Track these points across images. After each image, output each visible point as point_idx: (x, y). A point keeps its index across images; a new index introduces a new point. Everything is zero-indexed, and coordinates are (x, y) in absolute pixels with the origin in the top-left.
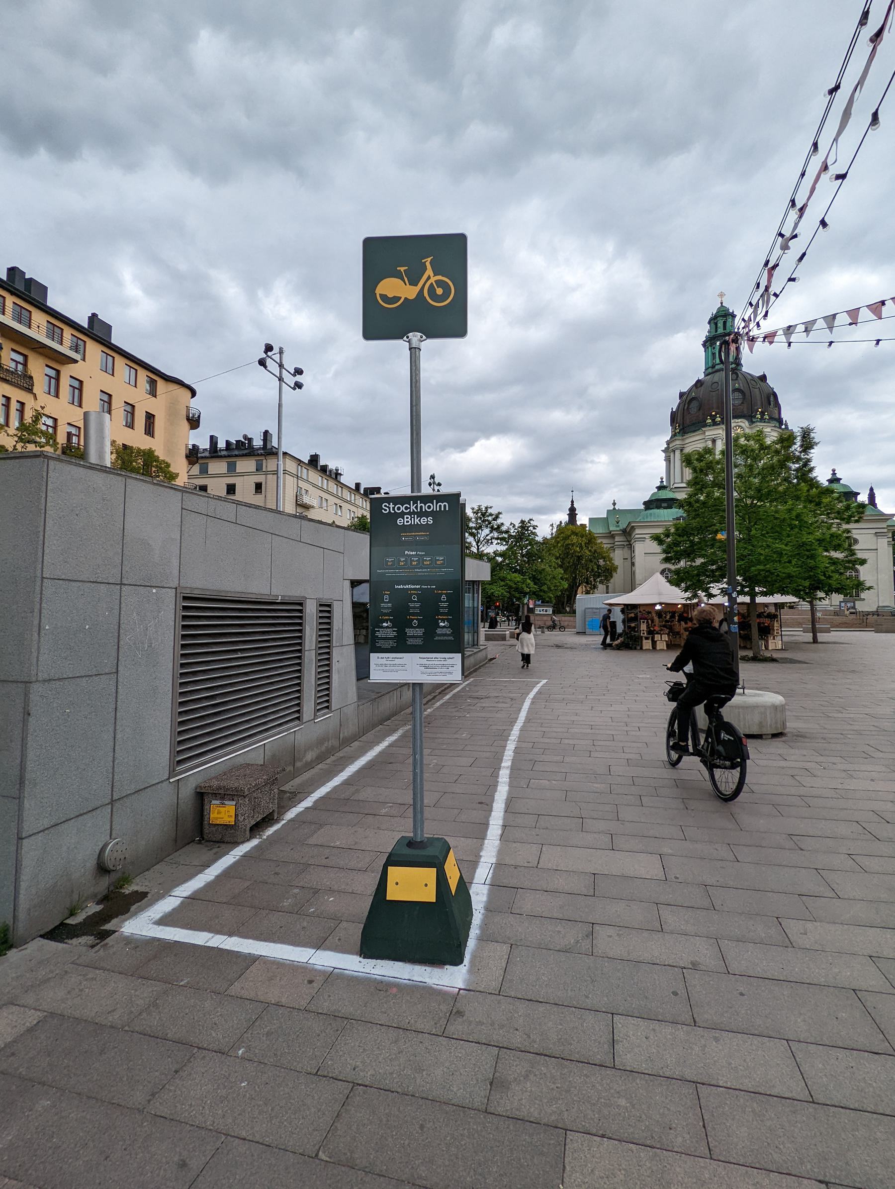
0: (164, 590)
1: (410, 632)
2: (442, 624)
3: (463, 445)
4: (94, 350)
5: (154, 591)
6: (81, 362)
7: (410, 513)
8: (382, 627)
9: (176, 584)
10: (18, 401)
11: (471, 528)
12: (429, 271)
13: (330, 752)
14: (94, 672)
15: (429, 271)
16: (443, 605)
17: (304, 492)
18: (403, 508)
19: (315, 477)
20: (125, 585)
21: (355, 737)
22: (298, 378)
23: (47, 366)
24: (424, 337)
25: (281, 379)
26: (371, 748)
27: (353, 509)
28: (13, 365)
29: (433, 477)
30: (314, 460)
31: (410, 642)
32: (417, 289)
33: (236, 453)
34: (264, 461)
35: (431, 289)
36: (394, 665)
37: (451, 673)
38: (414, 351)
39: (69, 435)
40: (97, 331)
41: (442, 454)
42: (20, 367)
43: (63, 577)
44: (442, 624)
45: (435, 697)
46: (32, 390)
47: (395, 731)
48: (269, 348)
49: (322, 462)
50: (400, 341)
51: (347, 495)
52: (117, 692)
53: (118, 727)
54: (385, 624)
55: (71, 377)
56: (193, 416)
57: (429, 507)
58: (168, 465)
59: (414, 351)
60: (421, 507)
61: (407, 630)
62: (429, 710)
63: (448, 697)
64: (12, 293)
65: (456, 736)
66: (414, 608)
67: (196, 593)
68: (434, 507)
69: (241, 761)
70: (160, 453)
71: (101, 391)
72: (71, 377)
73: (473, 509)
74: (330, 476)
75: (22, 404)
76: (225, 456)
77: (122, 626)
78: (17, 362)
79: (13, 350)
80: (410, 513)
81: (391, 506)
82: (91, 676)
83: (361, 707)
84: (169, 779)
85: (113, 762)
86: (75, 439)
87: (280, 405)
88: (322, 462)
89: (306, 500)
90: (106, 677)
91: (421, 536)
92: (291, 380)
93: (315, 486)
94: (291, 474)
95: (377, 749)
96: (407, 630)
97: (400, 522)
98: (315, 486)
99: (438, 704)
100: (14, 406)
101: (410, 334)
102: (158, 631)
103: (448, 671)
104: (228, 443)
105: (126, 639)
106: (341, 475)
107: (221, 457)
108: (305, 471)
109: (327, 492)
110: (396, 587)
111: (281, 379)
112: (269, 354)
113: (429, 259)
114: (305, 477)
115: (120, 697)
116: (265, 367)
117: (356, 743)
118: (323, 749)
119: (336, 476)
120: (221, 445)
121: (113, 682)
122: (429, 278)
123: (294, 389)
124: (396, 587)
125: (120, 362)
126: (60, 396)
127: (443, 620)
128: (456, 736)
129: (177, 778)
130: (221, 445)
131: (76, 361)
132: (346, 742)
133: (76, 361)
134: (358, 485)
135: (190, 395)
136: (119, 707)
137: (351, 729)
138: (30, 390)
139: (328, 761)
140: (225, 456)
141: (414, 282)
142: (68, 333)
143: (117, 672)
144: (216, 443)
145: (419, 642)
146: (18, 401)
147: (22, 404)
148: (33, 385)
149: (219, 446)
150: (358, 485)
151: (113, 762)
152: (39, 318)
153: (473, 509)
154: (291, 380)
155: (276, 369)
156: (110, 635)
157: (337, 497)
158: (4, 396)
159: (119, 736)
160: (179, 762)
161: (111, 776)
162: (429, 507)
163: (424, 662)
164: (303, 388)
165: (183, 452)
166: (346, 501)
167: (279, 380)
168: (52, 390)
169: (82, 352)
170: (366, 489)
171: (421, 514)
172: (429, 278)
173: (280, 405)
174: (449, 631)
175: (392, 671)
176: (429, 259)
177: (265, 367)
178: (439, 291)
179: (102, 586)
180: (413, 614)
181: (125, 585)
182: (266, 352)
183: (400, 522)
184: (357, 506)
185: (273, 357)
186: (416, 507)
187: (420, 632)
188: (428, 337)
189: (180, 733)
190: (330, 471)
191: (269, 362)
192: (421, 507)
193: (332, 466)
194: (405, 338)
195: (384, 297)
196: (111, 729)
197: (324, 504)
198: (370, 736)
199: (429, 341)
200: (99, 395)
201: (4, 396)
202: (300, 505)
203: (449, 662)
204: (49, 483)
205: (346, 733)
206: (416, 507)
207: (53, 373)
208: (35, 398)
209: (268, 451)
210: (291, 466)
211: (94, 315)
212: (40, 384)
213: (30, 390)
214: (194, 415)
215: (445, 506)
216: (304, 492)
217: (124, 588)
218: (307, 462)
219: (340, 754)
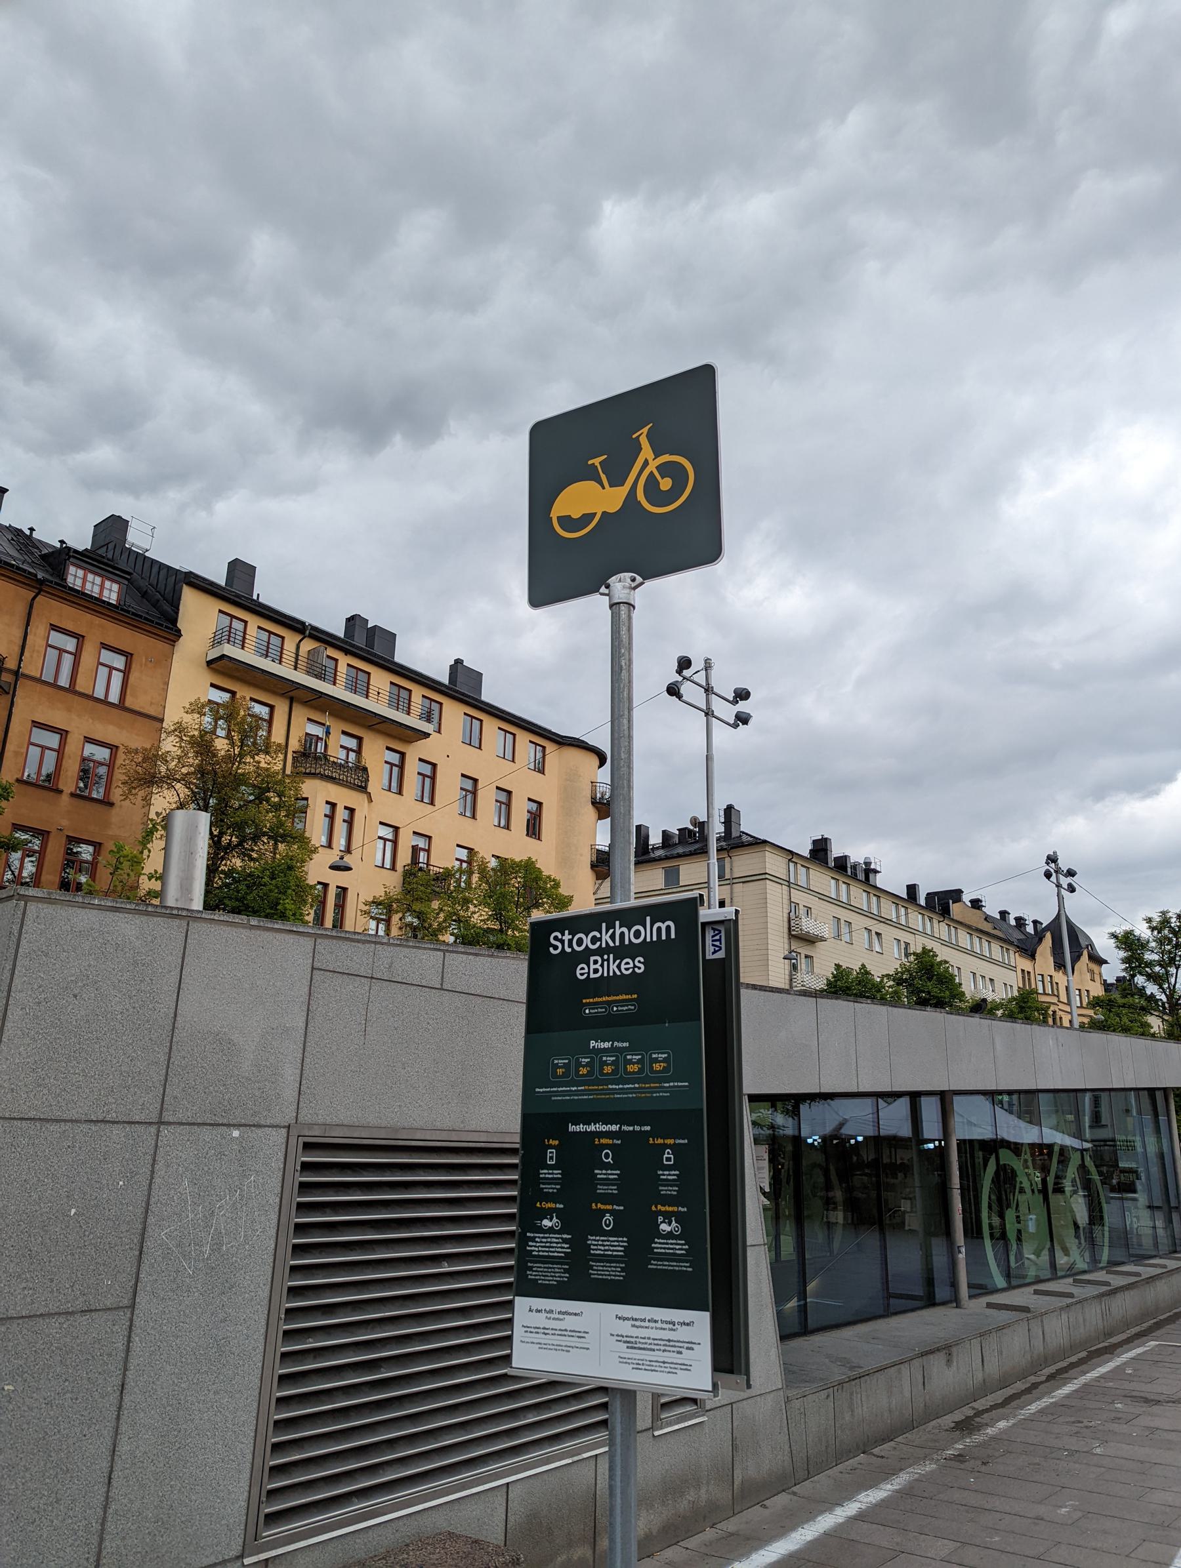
0: (259, 1131)
1: (598, 1245)
2: (664, 1227)
3: (1145, 785)
4: (454, 714)
5: (236, 1133)
6: (434, 735)
7: (600, 952)
8: (541, 1230)
9: (289, 1117)
10: (346, 808)
11: (1150, 964)
12: (647, 452)
13: (707, 1515)
14: (79, 1304)
15: (647, 452)
16: (665, 1175)
17: (802, 911)
18: (587, 941)
19: (822, 880)
20: (169, 1123)
21: (782, 1482)
22: (742, 706)
23: (388, 748)
24: (639, 579)
25: (709, 713)
26: (811, 1516)
27: (905, 937)
28: (342, 754)
29: (1052, 859)
30: (820, 849)
31: (600, 1271)
32: (622, 492)
33: (680, 850)
34: (727, 860)
35: (652, 482)
36: (563, 1332)
37: (686, 1367)
38: (620, 611)
39: (415, 850)
40: (462, 686)
41: (1098, 806)
42: (352, 756)
43: (32, 1114)
44: (664, 1227)
45: (1035, 1386)
46: (366, 788)
47: (888, 1474)
48: (684, 664)
49: (836, 851)
50: (596, 597)
51: (889, 910)
52: (128, 1350)
53: (124, 1428)
54: (546, 1223)
55: (420, 760)
56: (602, 798)
57: (637, 934)
58: (557, 885)
59: (620, 611)
60: (622, 934)
61: (592, 1240)
62: (1002, 1424)
63: (1067, 1389)
64: (347, 652)
65: (1042, 1510)
66: (607, 1182)
67: (337, 1136)
68: (648, 932)
69: (441, 1523)
70: (548, 866)
71: (463, 775)
72: (420, 760)
73: (1149, 920)
74: (854, 877)
75: (352, 811)
76: (660, 859)
77: (153, 1207)
78: (348, 750)
79: (344, 733)
80: (600, 952)
81: (567, 937)
82: (72, 1313)
83: (797, 1404)
84: (241, 1556)
85: (105, 1508)
86: (422, 857)
87: (709, 758)
88: (836, 851)
89: (808, 925)
90: (105, 1315)
91: (623, 1003)
92: (726, 711)
93: (823, 897)
94: (777, 880)
95: (826, 1522)
96: (592, 1240)
97: (581, 972)
98: (823, 897)
99: (1034, 1408)
100: (341, 814)
101: (612, 580)
102: (241, 1218)
103: (678, 1359)
104: (666, 835)
105: (159, 1235)
106: (876, 872)
107: (655, 860)
108: (802, 871)
109: (849, 907)
110: (572, 1128)
111: (709, 713)
112: (686, 673)
113: (645, 430)
114: (802, 881)
115: (133, 1362)
116: (679, 697)
117: (782, 1500)
118: (683, 1505)
119: (865, 875)
120: (655, 839)
121: (121, 1330)
122: (646, 463)
123: (735, 726)
124: (572, 1128)
125: (491, 726)
126: (404, 793)
127: (668, 1217)
128: (1042, 1510)
129: (263, 1556)
130: (655, 839)
131: (427, 735)
132: (753, 1493)
133: (427, 735)
134: (912, 890)
135: (597, 763)
136: (130, 1383)
137: (765, 1459)
138: (363, 788)
139: (693, 1542)
140: (660, 859)
141: (617, 480)
142: (418, 692)
143: (133, 1306)
144: (647, 837)
145: (614, 1272)
146: (346, 808)
147: (352, 811)
148: (367, 780)
149: (651, 842)
150: (912, 890)
151: (105, 1508)
152: (380, 680)
153: (1149, 920)
154: (726, 711)
155: (698, 697)
156: (124, 1228)
157: (868, 914)
158: (327, 802)
159: (124, 1447)
160: (273, 1518)
161: (95, 1540)
162: (637, 934)
163: (626, 1328)
164: (751, 722)
165: (587, 858)
166: (886, 921)
167: (707, 714)
168: (394, 784)
169: (436, 720)
170: (930, 896)
171: (622, 951)
172: (646, 463)
173: (709, 758)
174: (680, 1247)
175: (558, 1348)
176: (645, 430)
177: (679, 697)
178: (666, 484)
179: (116, 1130)
180: (606, 1198)
181: (169, 1123)
182: (679, 672)
183: (581, 972)
184: (913, 932)
185: (696, 678)
186: (613, 937)
187: (616, 1246)
188: (646, 577)
189: (277, 1447)
190: (855, 867)
191: (686, 689)
192: (622, 934)
193: (857, 855)
194: (603, 589)
195: (566, 521)
196: (107, 1433)
197: (844, 929)
198: (822, 1482)
199: (650, 584)
200: (458, 782)
201: (327, 802)
202: (794, 936)
203: (682, 1334)
204: (23, 942)
205: (751, 1468)
206: (613, 937)
207: (394, 758)
208: (370, 800)
209: (736, 842)
210: (774, 864)
211: (458, 662)
212: (378, 777)
213: (363, 788)
214: (603, 794)
215: (668, 928)
216: (802, 911)
217: (165, 1131)
218: (806, 854)
219: (731, 1526)
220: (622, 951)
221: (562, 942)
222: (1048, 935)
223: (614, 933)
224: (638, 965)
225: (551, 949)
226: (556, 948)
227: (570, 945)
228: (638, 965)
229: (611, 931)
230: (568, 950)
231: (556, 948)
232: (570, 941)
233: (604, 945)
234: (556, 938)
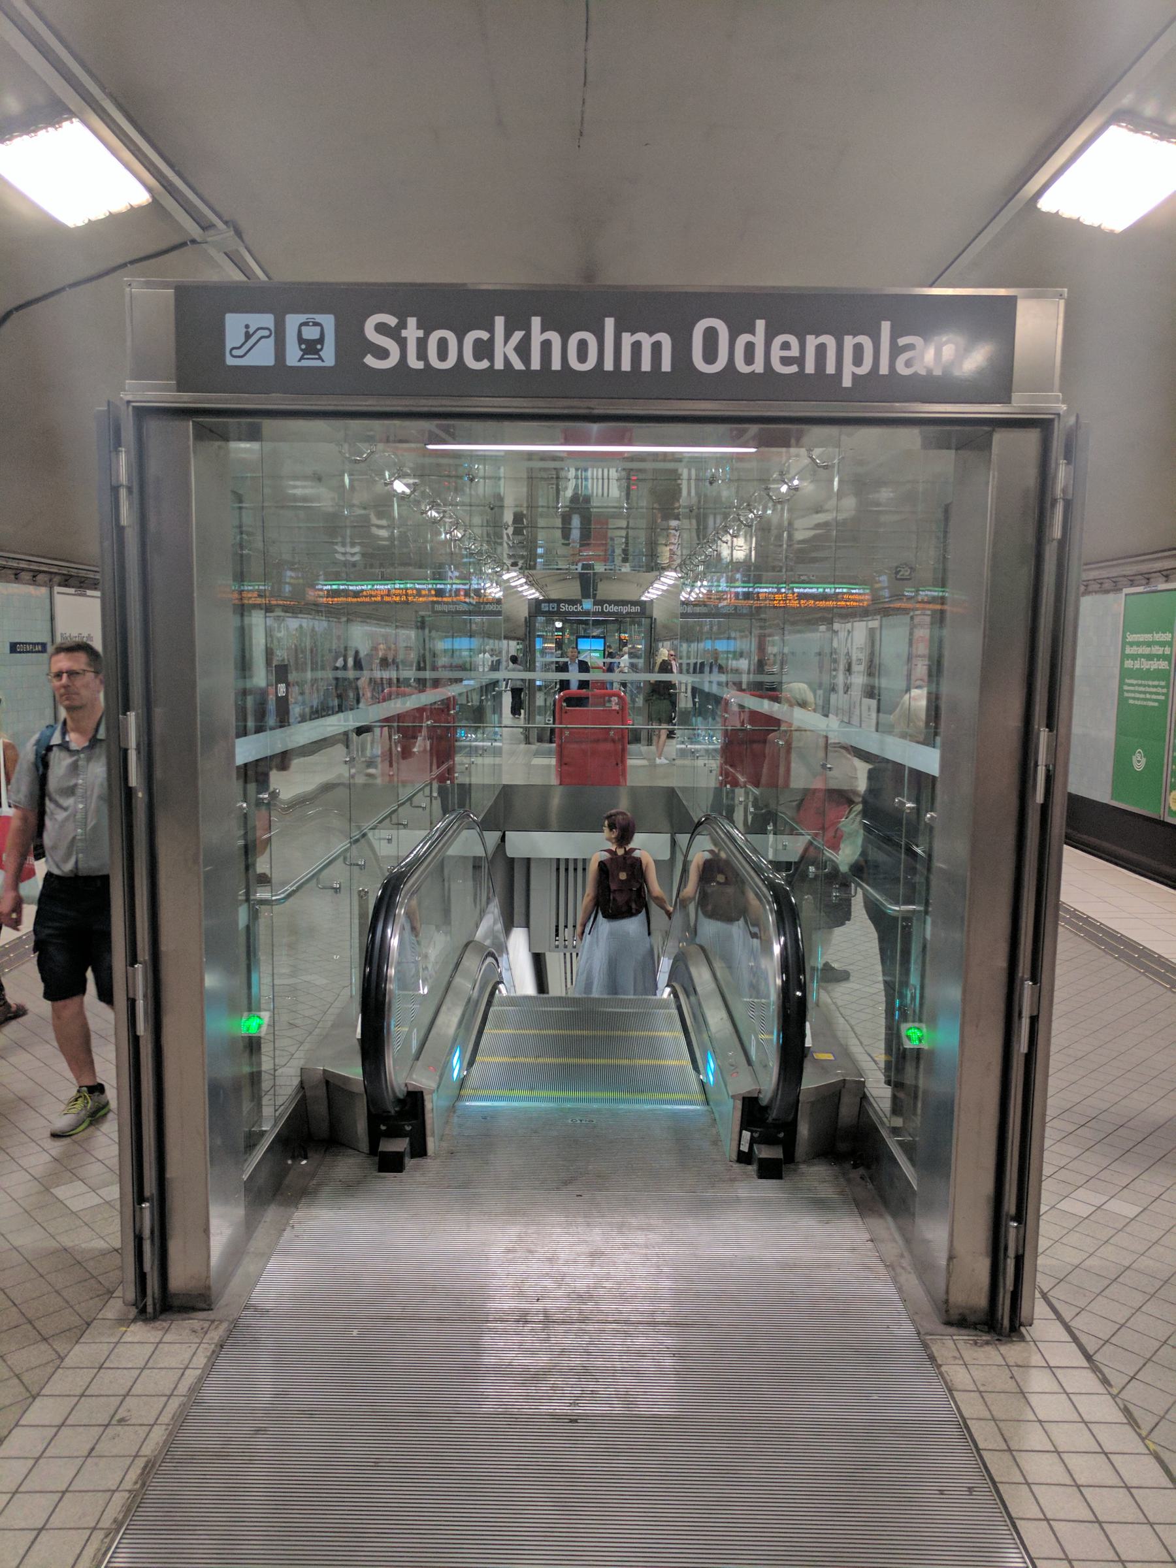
60: (546, 345)
81: (412, 332)
171: (1155, 701)
186: (523, 350)
192: (546, 345)
206: (523, 350)
215: (657, 347)
220: (1155, 701)
221: (402, 343)
222: (225, 1325)
223: (526, 340)
224: (1156, 704)
225: (370, 361)
226: (383, 354)
227: (422, 354)
228: (1156, 704)
229: (518, 335)
230: (415, 363)
231: (383, 354)
232: (422, 344)
233: (499, 365)
234: (381, 328)
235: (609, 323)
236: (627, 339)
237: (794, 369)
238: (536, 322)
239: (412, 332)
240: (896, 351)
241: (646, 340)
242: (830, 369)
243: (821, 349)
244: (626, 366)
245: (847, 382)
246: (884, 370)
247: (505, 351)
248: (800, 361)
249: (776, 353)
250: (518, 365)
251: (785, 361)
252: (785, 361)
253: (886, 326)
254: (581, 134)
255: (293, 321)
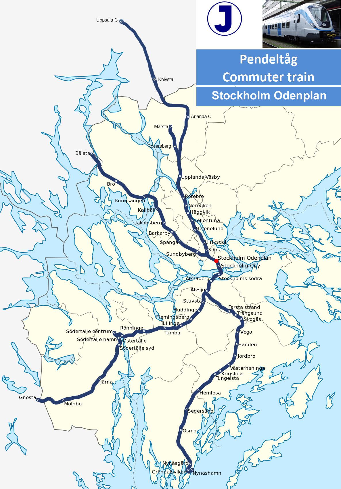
60: (247, 96)
81: (221, 94)
186: (242, 96)
192: (247, 96)
206: (242, 96)
215: (267, 96)
221: (219, 96)
227: (223, 97)
229: (241, 94)
232: (223, 96)
233: (238, 99)
234: (215, 93)
235: (259, 92)
236: (262, 95)
237: (274, 63)
238: (245, 92)
239: (221, 94)
240: (313, 96)
241: (265, 95)
242: (301, 99)
243: (299, 96)
244: (262, 99)
245: (305, 101)
246: (312, 99)
247: (239, 96)
248: (254, 61)
249: (270, 60)
250: (242, 99)
251: (272, 61)
252: (272, 61)
253: (312, 92)
254: (327, 176)
255: (302, 80)
